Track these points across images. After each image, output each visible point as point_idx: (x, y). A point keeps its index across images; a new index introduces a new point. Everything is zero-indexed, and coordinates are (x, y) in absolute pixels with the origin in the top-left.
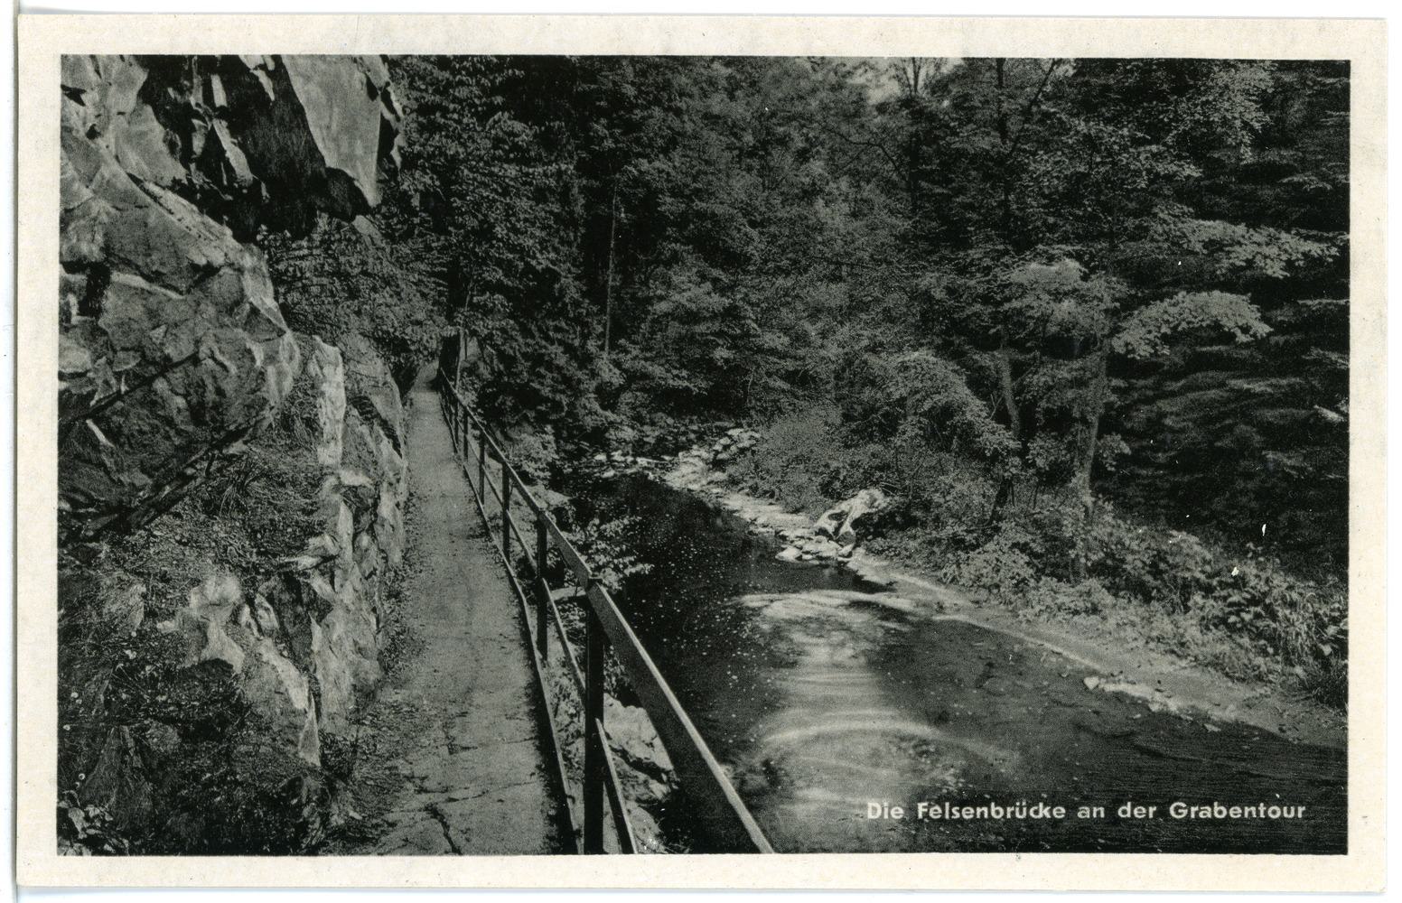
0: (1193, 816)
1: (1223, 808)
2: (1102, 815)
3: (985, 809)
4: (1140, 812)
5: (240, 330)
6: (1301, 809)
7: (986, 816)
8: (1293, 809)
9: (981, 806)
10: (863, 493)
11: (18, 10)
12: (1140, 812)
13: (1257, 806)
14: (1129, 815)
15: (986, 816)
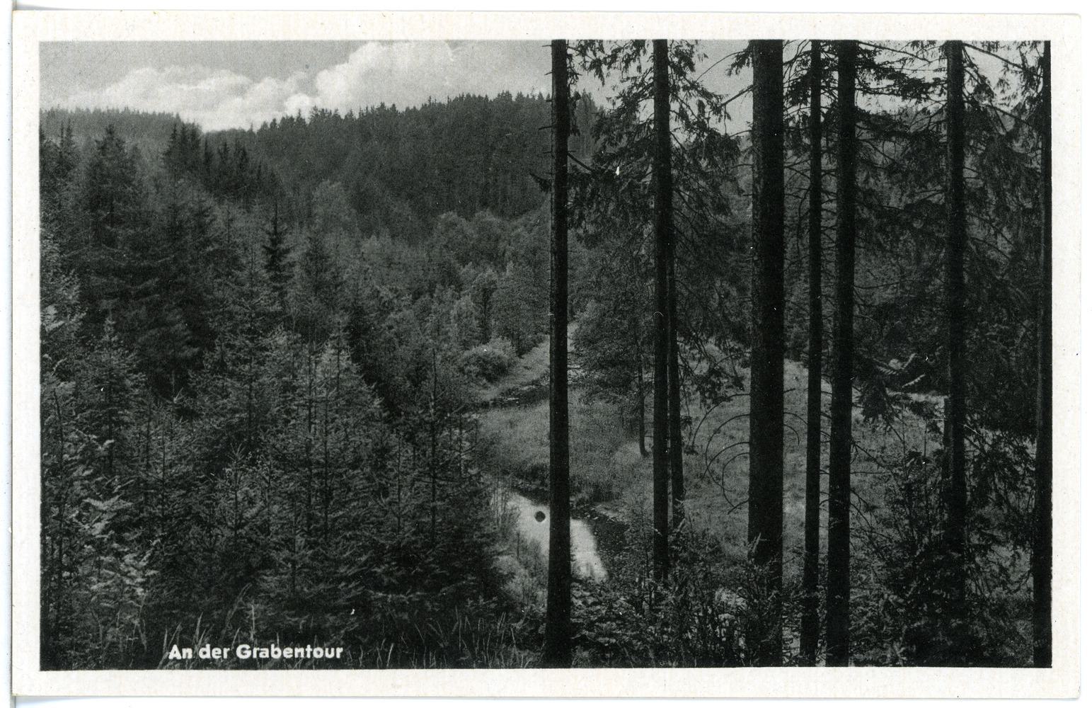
0: (255, 656)
3: (302, 650)
6: (340, 650)
8: (333, 650)
13: (305, 647)
14: (208, 656)
15: (302, 656)
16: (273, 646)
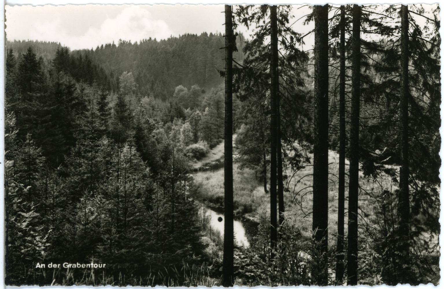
1: (79, 264)
2: (44, 267)
4: (55, 266)
5: (183, 125)
6: (104, 265)
7: (89, 267)
8: (102, 265)
9: (88, 264)
10: (47, 204)
11: (6, 4)
12: (55, 266)
14: (51, 267)
16: (77, 263)
